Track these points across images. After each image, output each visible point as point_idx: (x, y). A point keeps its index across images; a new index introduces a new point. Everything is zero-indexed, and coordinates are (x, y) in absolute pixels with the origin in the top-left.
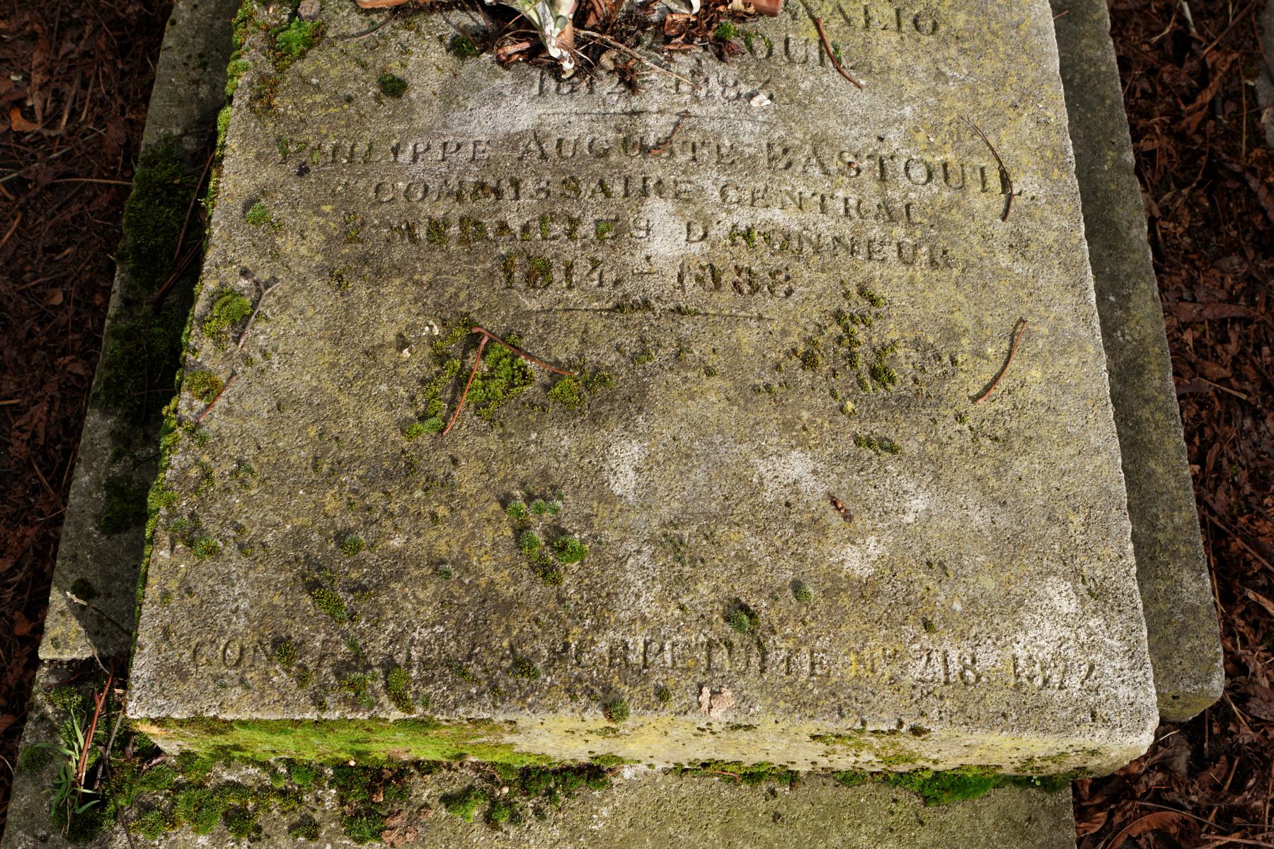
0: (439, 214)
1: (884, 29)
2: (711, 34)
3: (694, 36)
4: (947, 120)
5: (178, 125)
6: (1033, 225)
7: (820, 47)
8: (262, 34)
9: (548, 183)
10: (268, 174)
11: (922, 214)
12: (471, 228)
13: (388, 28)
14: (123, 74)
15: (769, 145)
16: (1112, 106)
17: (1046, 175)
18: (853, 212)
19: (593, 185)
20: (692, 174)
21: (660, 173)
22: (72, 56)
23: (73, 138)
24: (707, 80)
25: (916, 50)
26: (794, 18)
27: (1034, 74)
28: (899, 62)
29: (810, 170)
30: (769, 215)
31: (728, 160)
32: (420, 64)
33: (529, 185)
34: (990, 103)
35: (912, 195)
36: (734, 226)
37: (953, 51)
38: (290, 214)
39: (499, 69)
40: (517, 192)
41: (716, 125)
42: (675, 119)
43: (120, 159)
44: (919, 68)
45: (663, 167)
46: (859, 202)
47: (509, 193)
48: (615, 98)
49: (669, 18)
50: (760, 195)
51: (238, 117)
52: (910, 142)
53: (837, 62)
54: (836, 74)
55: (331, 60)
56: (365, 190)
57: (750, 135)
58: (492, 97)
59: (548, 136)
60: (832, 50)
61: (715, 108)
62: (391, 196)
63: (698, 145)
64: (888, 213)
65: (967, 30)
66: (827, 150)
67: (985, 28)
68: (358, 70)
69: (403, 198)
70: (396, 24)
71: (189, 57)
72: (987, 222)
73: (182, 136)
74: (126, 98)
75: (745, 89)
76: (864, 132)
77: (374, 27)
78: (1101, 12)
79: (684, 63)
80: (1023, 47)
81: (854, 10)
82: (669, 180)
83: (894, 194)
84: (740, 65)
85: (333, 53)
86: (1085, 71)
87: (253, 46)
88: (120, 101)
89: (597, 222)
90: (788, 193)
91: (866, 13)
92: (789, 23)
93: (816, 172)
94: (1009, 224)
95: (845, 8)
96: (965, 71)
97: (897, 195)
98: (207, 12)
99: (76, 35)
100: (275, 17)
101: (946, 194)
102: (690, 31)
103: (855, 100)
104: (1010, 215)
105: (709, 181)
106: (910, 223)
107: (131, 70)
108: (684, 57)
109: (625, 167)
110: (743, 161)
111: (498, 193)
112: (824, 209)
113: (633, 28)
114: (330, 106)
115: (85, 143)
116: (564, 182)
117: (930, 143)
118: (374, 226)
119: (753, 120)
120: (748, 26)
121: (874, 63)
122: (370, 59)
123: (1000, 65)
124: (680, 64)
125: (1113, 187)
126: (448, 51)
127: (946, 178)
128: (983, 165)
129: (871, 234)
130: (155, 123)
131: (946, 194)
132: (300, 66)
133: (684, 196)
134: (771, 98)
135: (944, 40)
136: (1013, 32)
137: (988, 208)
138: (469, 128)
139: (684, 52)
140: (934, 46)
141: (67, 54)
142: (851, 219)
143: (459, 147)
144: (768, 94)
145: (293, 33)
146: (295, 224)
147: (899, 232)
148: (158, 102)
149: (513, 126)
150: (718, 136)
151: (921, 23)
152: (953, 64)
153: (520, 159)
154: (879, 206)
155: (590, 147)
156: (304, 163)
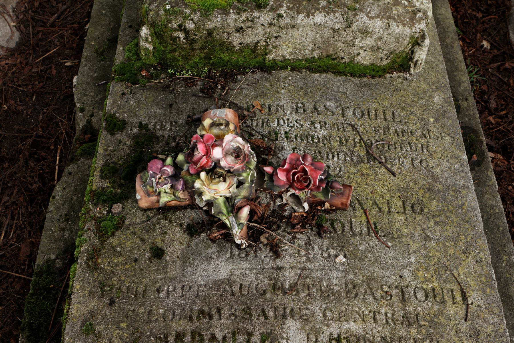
0: (180, 328)
1: (398, 213)
2: (314, 222)
3: (307, 223)
4: (432, 263)
5: (53, 254)
6: (481, 322)
7: (367, 225)
8: (93, 222)
9: (236, 310)
10: (94, 304)
11: (425, 320)
12: (197, 338)
13: (155, 219)
14: (31, 214)
15: (346, 284)
16: (503, 231)
17: (484, 292)
18: (390, 321)
19: (258, 312)
20: (308, 304)
21: (292, 305)
22: (8, 204)
23: (5, 247)
24: (313, 248)
25: (414, 224)
26: (354, 209)
27: (472, 233)
28: (406, 231)
29: (367, 298)
30: (348, 326)
31: (327, 294)
32: (171, 240)
33: (226, 312)
34: (452, 252)
35: (419, 309)
36: (331, 334)
37: (432, 223)
38: (105, 328)
39: (210, 243)
40: (220, 315)
41: (319, 274)
42: (299, 272)
43: (27, 263)
44: (416, 234)
45: (294, 301)
46: (393, 315)
47: (216, 316)
48: (268, 260)
49: (293, 214)
50: (343, 314)
51: (80, 270)
52: (415, 277)
53: (376, 233)
54: (377, 240)
55: (127, 237)
56: (143, 313)
57: (336, 278)
58: (207, 258)
59: (235, 282)
60: (373, 226)
61: (318, 264)
62: (156, 317)
63: (311, 286)
64: (408, 321)
65: (437, 211)
66: (375, 285)
67: (446, 209)
68: (140, 243)
69: (162, 319)
70: (159, 217)
71: (61, 216)
72: (457, 322)
73: (55, 259)
74: (31, 227)
75: (333, 252)
76: (393, 273)
77: (149, 218)
78: (493, 181)
79: (302, 239)
80: (465, 219)
81: (383, 203)
82: (296, 308)
83: (410, 309)
84: (329, 238)
85: (128, 233)
86: (488, 212)
87: (89, 229)
88: (29, 229)
89: (262, 334)
90: (357, 312)
91: (388, 204)
92: (352, 212)
93: (370, 298)
94: (469, 323)
95: (378, 202)
96: (439, 234)
97: (411, 309)
98: (70, 191)
99: (10, 193)
100: (100, 213)
101: (436, 307)
102: (304, 221)
103: (388, 255)
104: (469, 318)
105: (316, 308)
106: (419, 326)
107: (35, 212)
108: (301, 235)
109: (274, 301)
110: (334, 294)
111: (211, 317)
112: (375, 320)
113: (276, 220)
114: (126, 263)
115: (11, 250)
116: (244, 310)
117: (425, 277)
118: (147, 336)
119: (337, 270)
120: (332, 216)
121: (395, 233)
122: (146, 237)
123: (455, 229)
124: (299, 239)
125: (508, 276)
126: (185, 232)
127: (435, 297)
128: (452, 288)
129: (400, 334)
130: (43, 253)
131: (436, 307)
132: (112, 240)
133: (305, 317)
134: (345, 256)
135: (427, 217)
136: (460, 211)
137: (457, 313)
138: (195, 277)
139: (302, 233)
140: (423, 221)
141: (5, 202)
142: (390, 325)
143: (190, 288)
144: (343, 254)
145: (107, 223)
146: (107, 334)
147: (414, 331)
148: (45, 242)
149: (218, 276)
150: (320, 281)
151: (415, 208)
152: (433, 231)
153: (221, 295)
154: (403, 317)
155: (256, 288)
156: (113, 298)
